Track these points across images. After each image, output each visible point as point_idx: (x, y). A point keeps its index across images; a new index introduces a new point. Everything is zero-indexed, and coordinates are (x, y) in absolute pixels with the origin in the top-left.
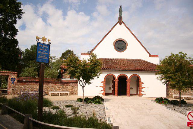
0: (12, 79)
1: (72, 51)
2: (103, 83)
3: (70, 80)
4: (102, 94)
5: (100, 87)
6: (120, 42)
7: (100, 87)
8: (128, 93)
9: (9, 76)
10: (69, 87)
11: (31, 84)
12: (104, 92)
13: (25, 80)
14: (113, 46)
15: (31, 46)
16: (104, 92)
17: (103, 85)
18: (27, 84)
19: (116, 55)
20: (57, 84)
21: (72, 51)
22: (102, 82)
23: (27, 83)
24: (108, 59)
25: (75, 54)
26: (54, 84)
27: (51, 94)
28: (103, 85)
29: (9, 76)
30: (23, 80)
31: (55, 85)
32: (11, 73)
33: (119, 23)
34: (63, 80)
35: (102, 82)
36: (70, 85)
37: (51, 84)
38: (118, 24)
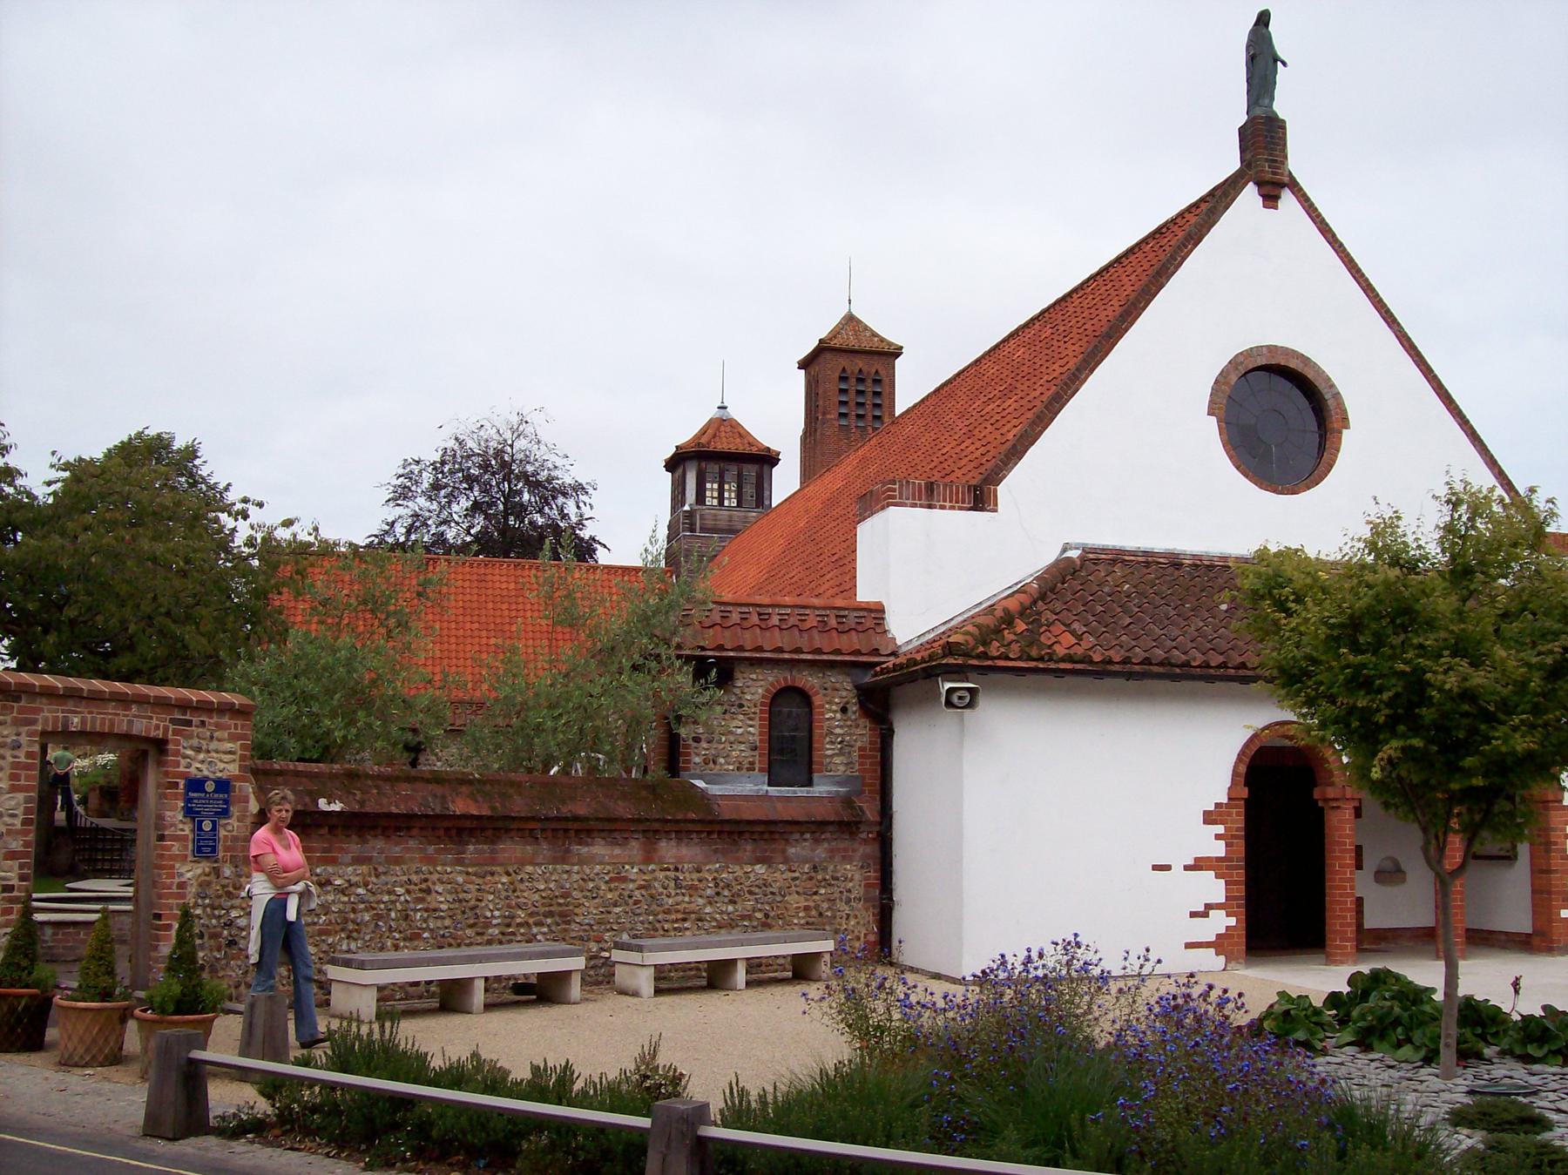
0: (196, 784)
1: (191, 453)
2: (1220, 829)
3: (773, 791)
4: (1220, 944)
5: (1199, 865)
6: (1286, 386)
7: (1199, 865)
8: (1339, 920)
9: (160, 745)
10: (779, 876)
11: (396, 850)
12: (1232, 921)
13: (337, 807)
14: (1211, 426)
15: (896, 352)
16: (1232, 921)
17: (1219, 850)
18: (358, 861)
19: (1222, 515)
20: (668, 850)
21: (191, 453)
22: (1209, 818)
23: (354, 847)
24: (1174, 561)
25: (220, 479)
26: (635, 848)
27: (661, 973)
28: (1219, 850)
29: (160, 745)
30: (323, 804)
31: (648, 860)
32: (184, 706)
33: (1259, 184)
34: (715, 790)
35: (1209, 818)
36: (792, 851)
37: (599, 849)
38: (1250, 194)
